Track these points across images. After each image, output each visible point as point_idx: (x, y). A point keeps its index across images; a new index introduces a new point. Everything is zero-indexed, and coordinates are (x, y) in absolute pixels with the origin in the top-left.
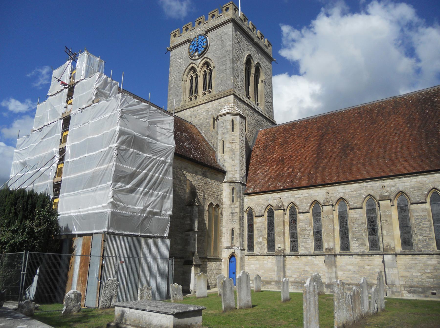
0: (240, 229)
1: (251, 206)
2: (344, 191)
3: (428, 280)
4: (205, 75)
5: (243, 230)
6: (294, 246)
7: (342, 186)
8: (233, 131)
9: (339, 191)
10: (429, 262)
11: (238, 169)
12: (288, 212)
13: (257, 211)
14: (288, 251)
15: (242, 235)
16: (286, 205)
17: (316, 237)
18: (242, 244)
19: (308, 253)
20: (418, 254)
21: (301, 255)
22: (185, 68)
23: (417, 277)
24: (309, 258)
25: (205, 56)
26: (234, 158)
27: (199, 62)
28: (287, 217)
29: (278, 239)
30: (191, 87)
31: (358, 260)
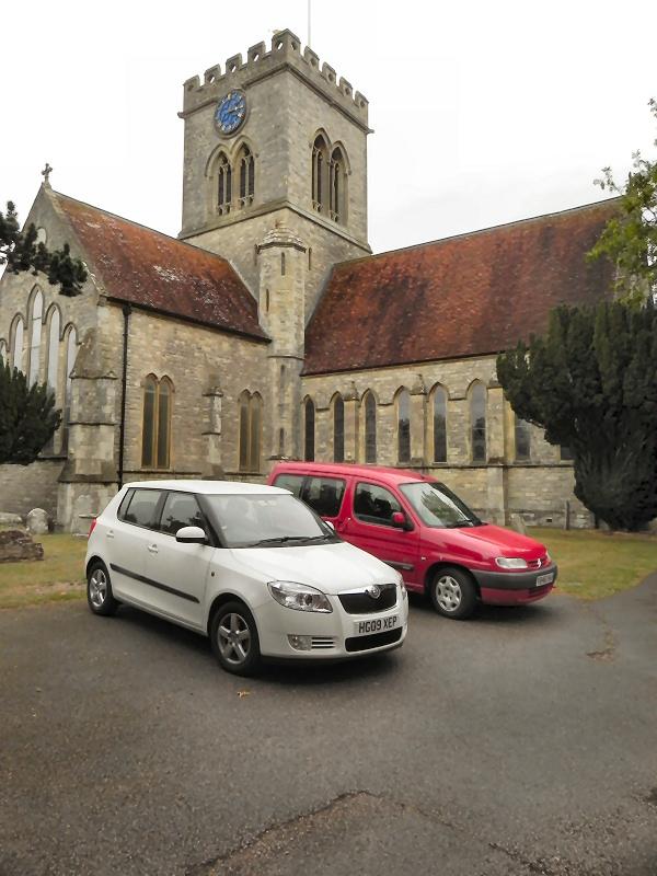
0: (293, 430)
1: (311, 393)
3: (544, 502)
4: (243, 168)
5: (298, 432)
8: (283, 274)
10: (549, 478)
11: (291, 336)
12: (363, 404)
13: (320, 402)
16: (361, 393)
18: (296, 451)
20: (535, 467)
22: (209, 154)
23: (530, 499)
25: (243, 133)
27: (231, 147)
28: (362, 411)
29: (348, 444)
30: (221, 189)
31: (456, 475)
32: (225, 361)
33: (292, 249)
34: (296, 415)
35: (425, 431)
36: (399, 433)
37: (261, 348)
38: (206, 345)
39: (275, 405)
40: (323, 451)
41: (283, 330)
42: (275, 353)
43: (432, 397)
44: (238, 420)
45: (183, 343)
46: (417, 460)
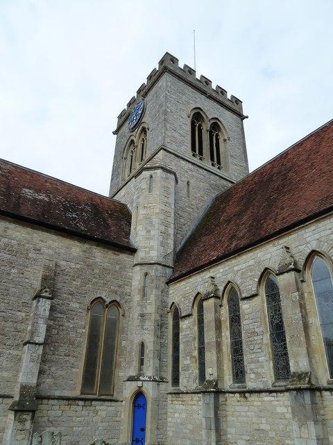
1: (176, 300)
2: (317, 236)
5: (162, 346)
6: (239, 374)
7: (313, 228)
9: (308, 239)
14: (228, 382)
15: (160, 356)
17: (276, 347)
18: (160, 368)
19: (261, 387)
21: (251, 392)
24: (267, 398)
26: (149, 228)
28: (225, 312)
32: (73, 265)
33: (159, 172)
34: (161, 326)
35: (306, 327)
36: (272, 334)
37: (124, 257)
38: (49, 248)
39: (136, 315)
40: (187, 368)
41: (148, 239)
42: (139, 261)
43: (308, 275)
44: (86, 331)
45: (14, 242)
46: (300, 376)
